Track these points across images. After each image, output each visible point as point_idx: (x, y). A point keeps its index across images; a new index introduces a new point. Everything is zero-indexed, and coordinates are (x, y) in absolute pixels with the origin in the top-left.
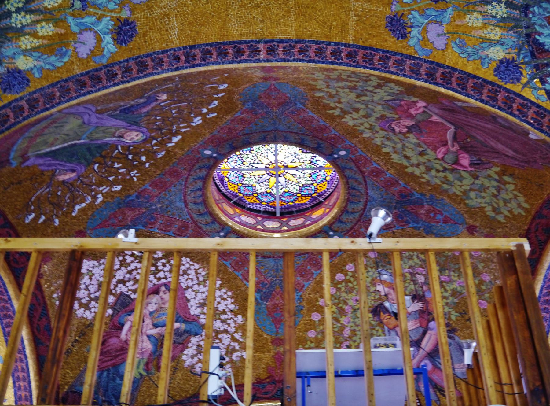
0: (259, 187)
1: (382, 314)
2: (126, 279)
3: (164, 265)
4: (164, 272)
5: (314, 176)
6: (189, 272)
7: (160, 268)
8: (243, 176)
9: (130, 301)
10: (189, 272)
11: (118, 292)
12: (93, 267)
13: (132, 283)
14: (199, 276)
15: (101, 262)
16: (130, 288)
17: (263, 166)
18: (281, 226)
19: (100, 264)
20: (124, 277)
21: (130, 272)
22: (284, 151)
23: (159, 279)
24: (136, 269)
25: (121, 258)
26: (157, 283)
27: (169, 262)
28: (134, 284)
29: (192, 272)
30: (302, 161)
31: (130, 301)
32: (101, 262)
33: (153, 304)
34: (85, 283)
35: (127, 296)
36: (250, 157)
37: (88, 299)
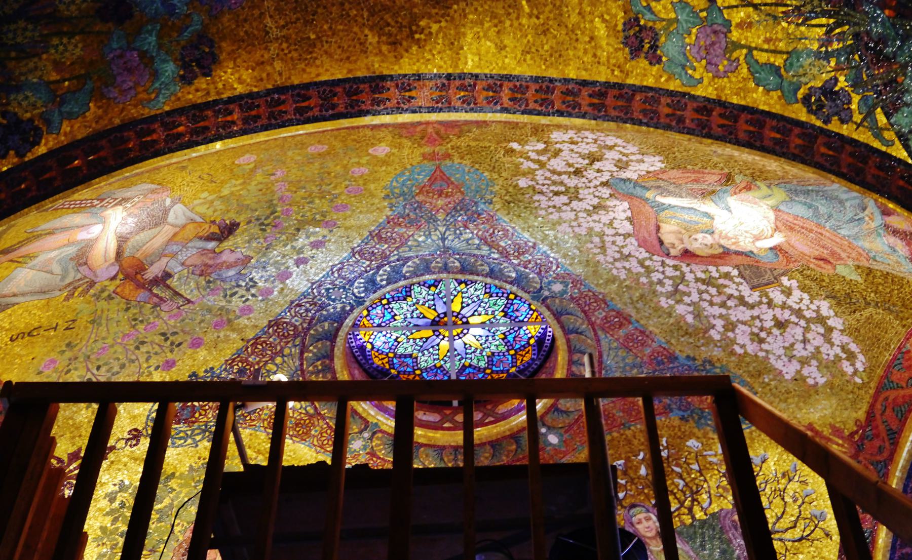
0: (478, 293)
1: (218, 231)
2: (736, 302)
3: (660, 282)
4: (663, 273)
5: (388, 316)
6: (617, 256)
7: (668, 282)
8: (506, 315)
9: (742, 268)
10: (617, 256)
11: (757, 293)
12: (780, 356)
13: (728, 291)
14: (600, 245)
15: (764, 354)
16: (734, 286)
17: (473, 331)
18: (442, 421)
19: (767, 351)
20: (736, 306)
21: (723, 305)
22: (441, 357)
23: (676, 268)
24: (712, 304)
25: (730, 334)
26: (684, 265)
27: (651, 283)
28: (725, 286)
29: (612, 251)
30: (411, 341)
31: (742, 268)
32: (764, 354)
33: (700, 240)
34: (805, 349)
35: (743, 277)
36: (493, 348)
37: (813, 327)
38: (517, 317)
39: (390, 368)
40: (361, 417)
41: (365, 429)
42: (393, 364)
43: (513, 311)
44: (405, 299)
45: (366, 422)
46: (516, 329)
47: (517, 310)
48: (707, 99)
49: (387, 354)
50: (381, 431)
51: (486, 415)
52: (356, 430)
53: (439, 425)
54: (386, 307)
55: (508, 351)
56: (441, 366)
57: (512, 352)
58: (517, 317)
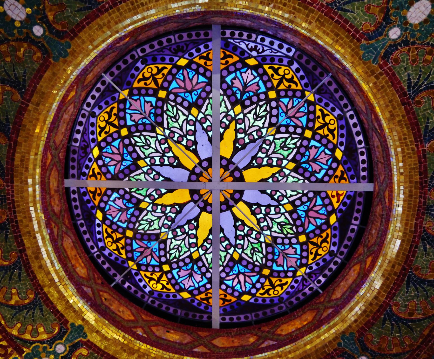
0: (260, 123)
18: (194, 344)
22: (200, 243)
38: (313, 173)
39: (128, 259)
40: (55, 311)
41: (59, 336)
42: (132, 251)
43: (307, 162)
44: (153, 130)
45: (62, 319)
46: (311, 195)
47: (314, 160)
48: (383, 285)
49: (124, 233)
50: (90, 345)
51: (261, 339)
52: (45, 337)
53: (187, 348)
54: (127, 141)
55: (297, 235)
56: (200, 259)
57: (302, 238)
58: (313, 173)
